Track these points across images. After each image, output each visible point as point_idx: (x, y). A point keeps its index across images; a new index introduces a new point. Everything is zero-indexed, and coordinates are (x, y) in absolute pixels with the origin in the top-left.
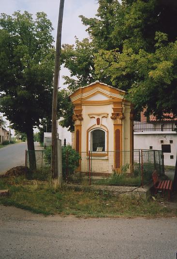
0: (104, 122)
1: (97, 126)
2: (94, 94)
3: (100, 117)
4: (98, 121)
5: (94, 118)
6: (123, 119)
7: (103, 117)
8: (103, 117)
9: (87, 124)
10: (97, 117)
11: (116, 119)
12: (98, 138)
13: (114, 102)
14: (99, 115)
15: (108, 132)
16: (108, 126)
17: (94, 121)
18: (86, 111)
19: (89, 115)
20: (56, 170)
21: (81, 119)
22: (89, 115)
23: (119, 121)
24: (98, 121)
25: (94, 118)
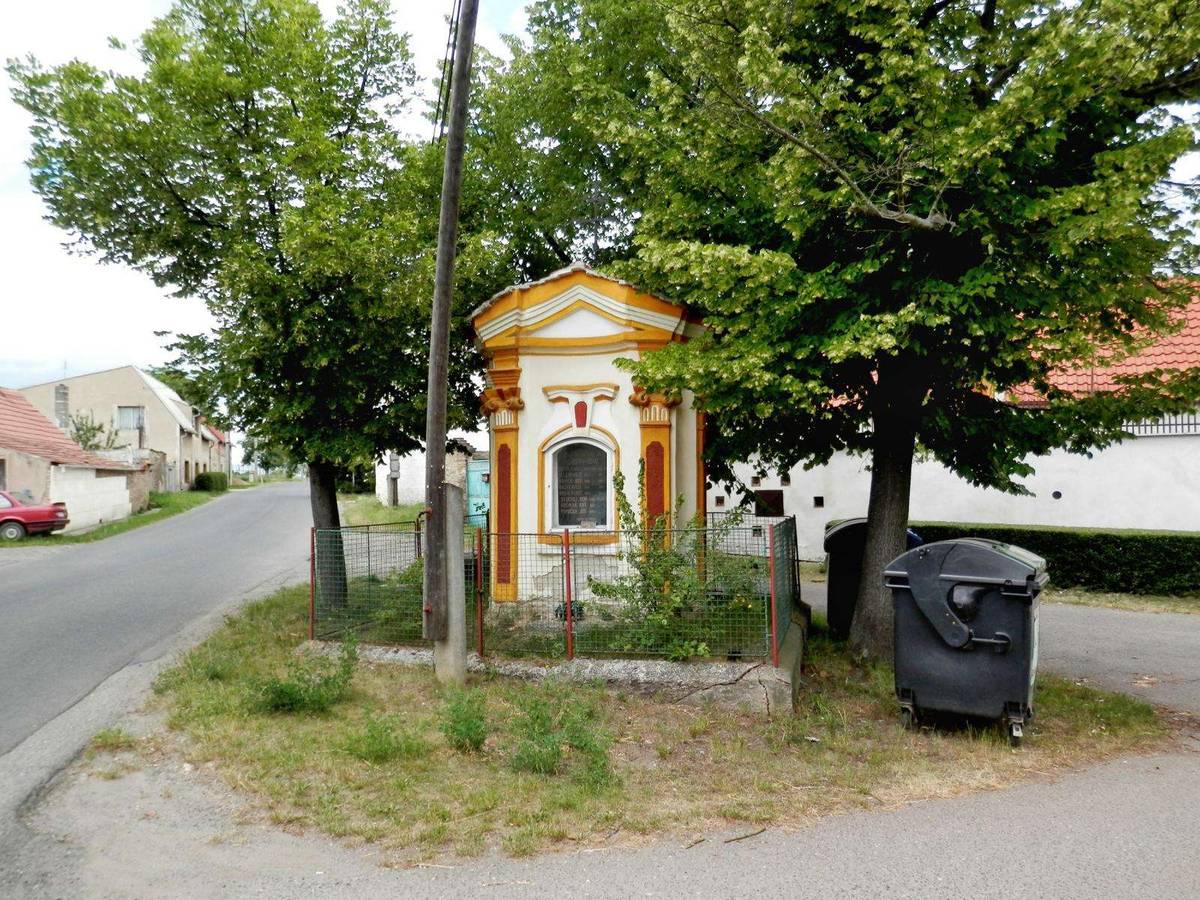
0: (600, 414)
1: (575, 431)
2: (565, 313)
3: (589, 400)
4: (581, 412)
5: (566, 400)
6: (673, 405)
7: (597, 399)
8: (597, 399)
9: (541, 426)
10: (575, 399)
11: (647, 404)
12: (580, 469)
13: (640, 342)
14: (582, 390)
15: (617, 452)
16: (621, 432)
17: (566, 414)
18: (533, 376)
20: (443, 608)
21: (517, 408)
22: (545, 391)
23: (658, 413)
24: (581, 412)
25: (566, 400)
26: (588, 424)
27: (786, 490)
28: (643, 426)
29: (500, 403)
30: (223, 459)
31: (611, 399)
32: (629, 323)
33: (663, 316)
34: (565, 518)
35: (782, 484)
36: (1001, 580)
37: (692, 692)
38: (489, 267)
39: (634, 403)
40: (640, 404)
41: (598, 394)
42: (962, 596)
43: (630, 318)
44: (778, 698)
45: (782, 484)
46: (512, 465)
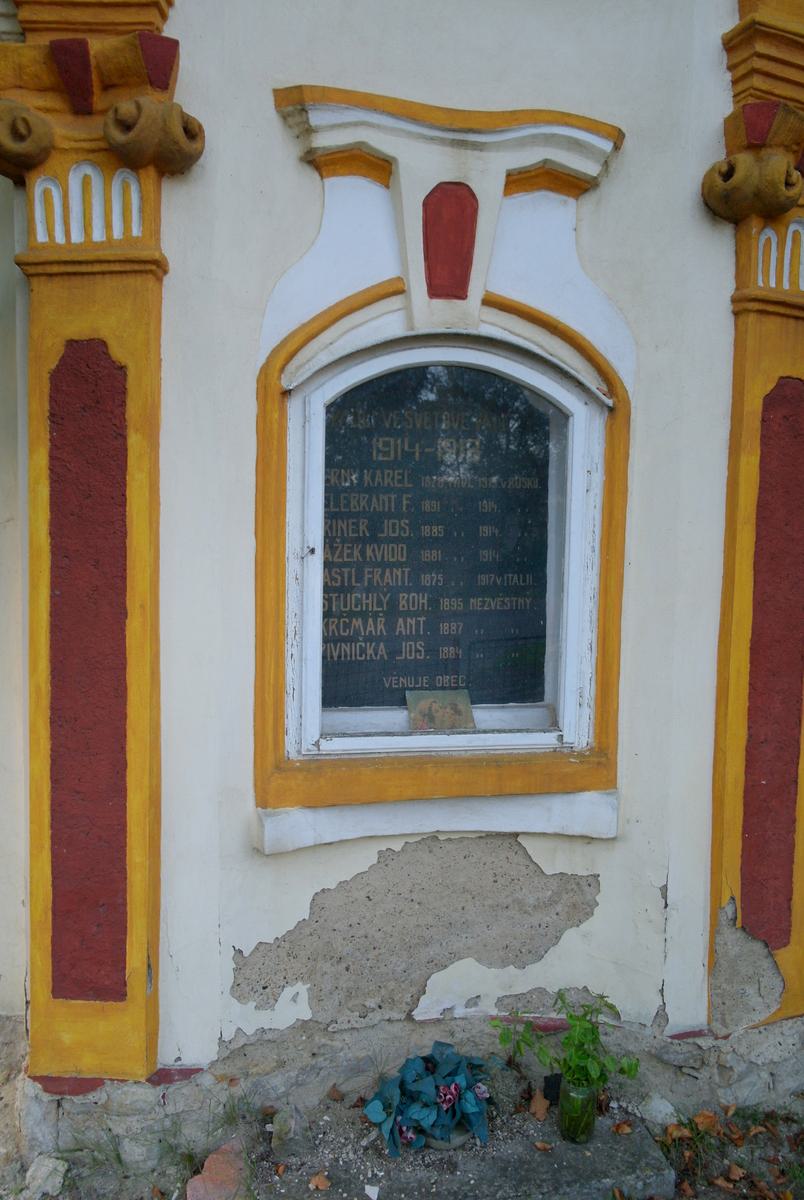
0: (528, 253)
1: (432, 314)
3: (485, 174)
5: (380, 168)
7: (518, 181)
8: (518, 181)
10: (425, 165)
11: (773, 211)
14: (462, 128)
15: (615, 409)
17: (364, 238)
19: (294, 104)
21: (168, 155)
25: (380, 168)
26: (476, 289)
28: (748, 305)
29: (60, 127)
31: (575, 185)
34: (345, 686)
39: (731, 205)
46: (134, 441)
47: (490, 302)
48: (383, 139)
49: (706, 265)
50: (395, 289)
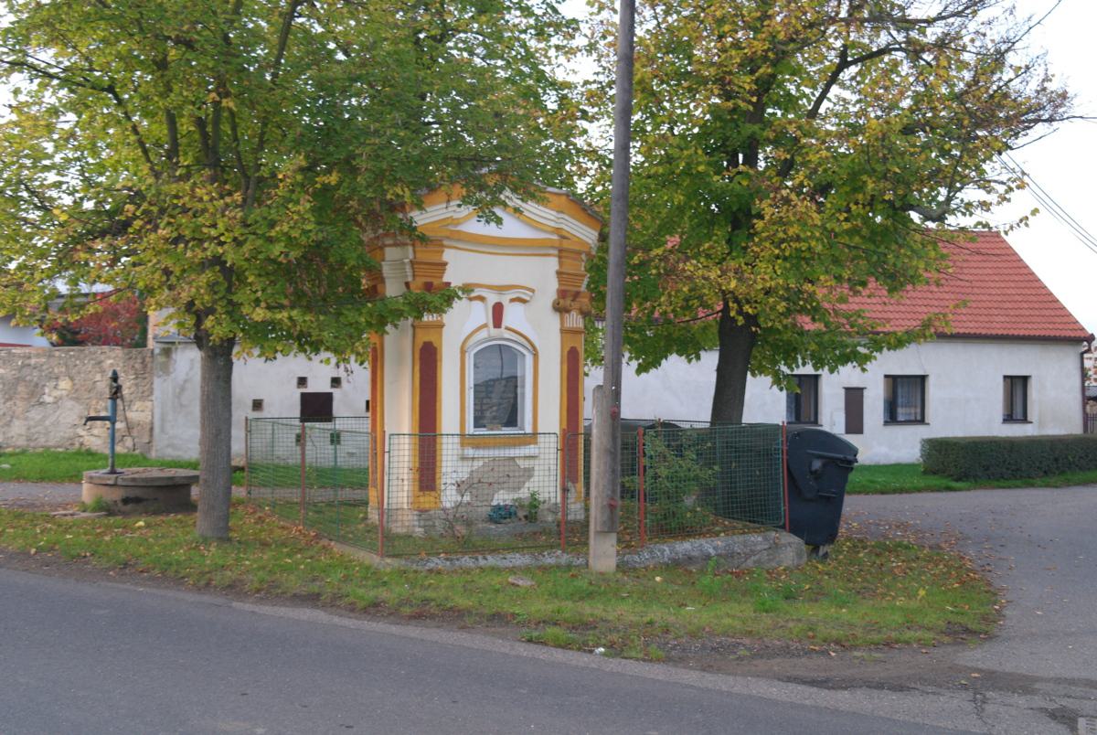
0: (513, 316)
3: (505, 299)
4: (498, 311)
7: (512, 300)
8: (512, 300)
9: (461, 326)
10: (493, 298)
14: (501, 289)
16: (540, 329)
24: (498, 311)
25: (481, 299)
26: (503, 326)
27: (336, 393)
28: (564, 331)
30: (979, 240)
31: (524, 301)
32: (557, 231)
33: (584, 227)
35: (332, 386)
36: (841, 456)
37: (746, 559)
38: (857, 26)
40: (559, 309)
41: (514, 296)
42: (817, 464)
43: (557, 226)
44: (799, 556)
45: (332, 386)
47: (507, 329)
48: (484, 293)
49: (554, 321)
50: (485, 326)
